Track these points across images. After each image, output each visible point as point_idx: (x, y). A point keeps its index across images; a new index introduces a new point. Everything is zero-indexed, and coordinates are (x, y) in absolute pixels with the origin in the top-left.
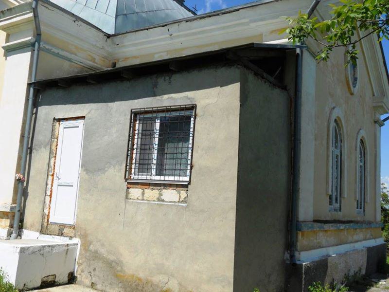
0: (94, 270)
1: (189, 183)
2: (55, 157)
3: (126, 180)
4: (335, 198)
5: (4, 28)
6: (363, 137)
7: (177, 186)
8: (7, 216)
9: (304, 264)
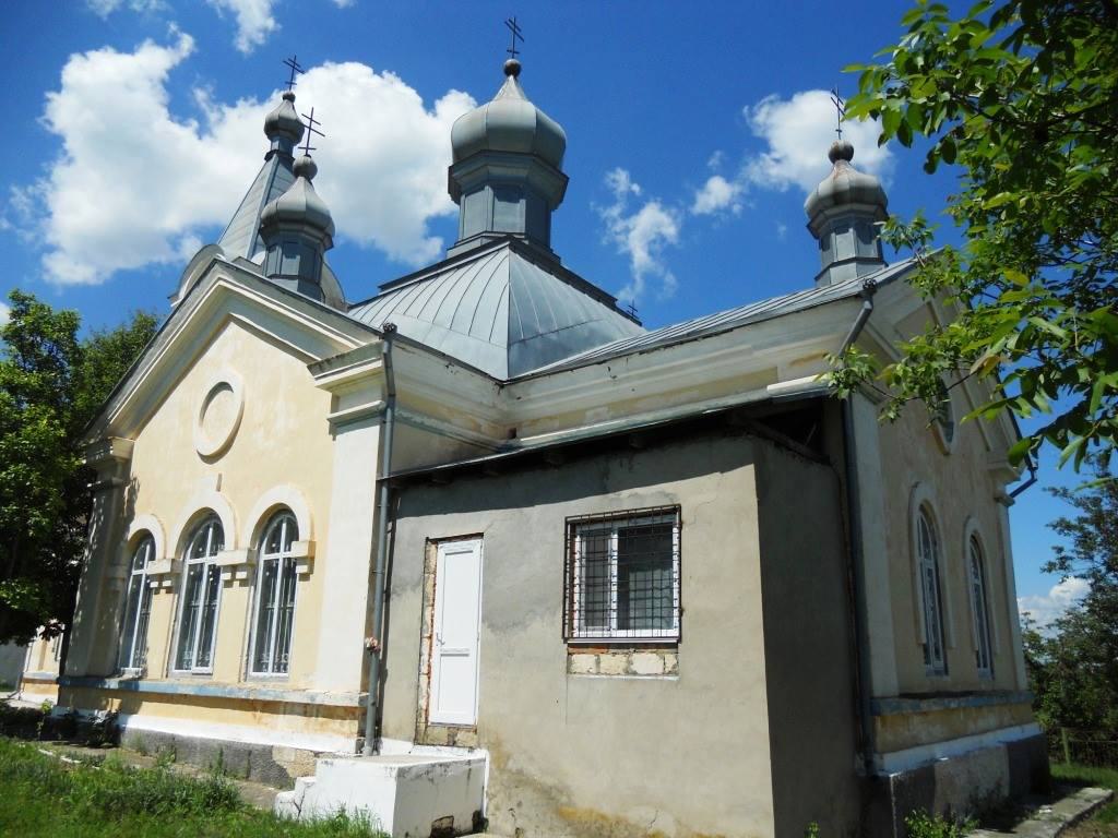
0: (519, 804)
1: (680, 639)
2: (433, 605)
3: (565, 640)
4: (935, 649)
5: (328, 387)
6: (975, 531)
7: (658, 646)
8: (353, 714)
9: (892, 776)
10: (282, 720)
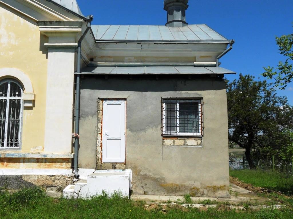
2: (102, 122)
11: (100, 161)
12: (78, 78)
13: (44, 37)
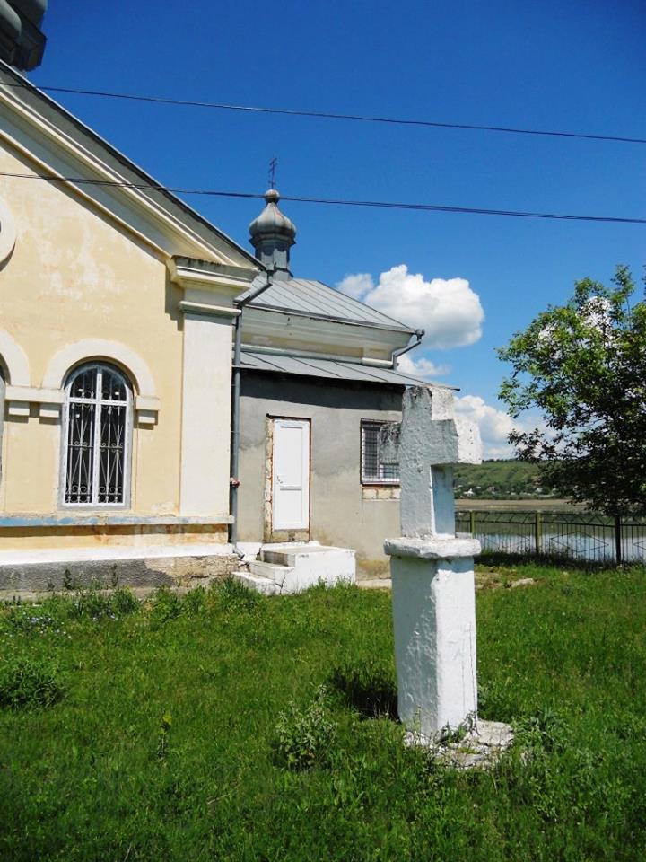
2: (271, 458)
10: (137, 539)
11: (270, 529)
12: (238, 375)
13: (175, 288)
